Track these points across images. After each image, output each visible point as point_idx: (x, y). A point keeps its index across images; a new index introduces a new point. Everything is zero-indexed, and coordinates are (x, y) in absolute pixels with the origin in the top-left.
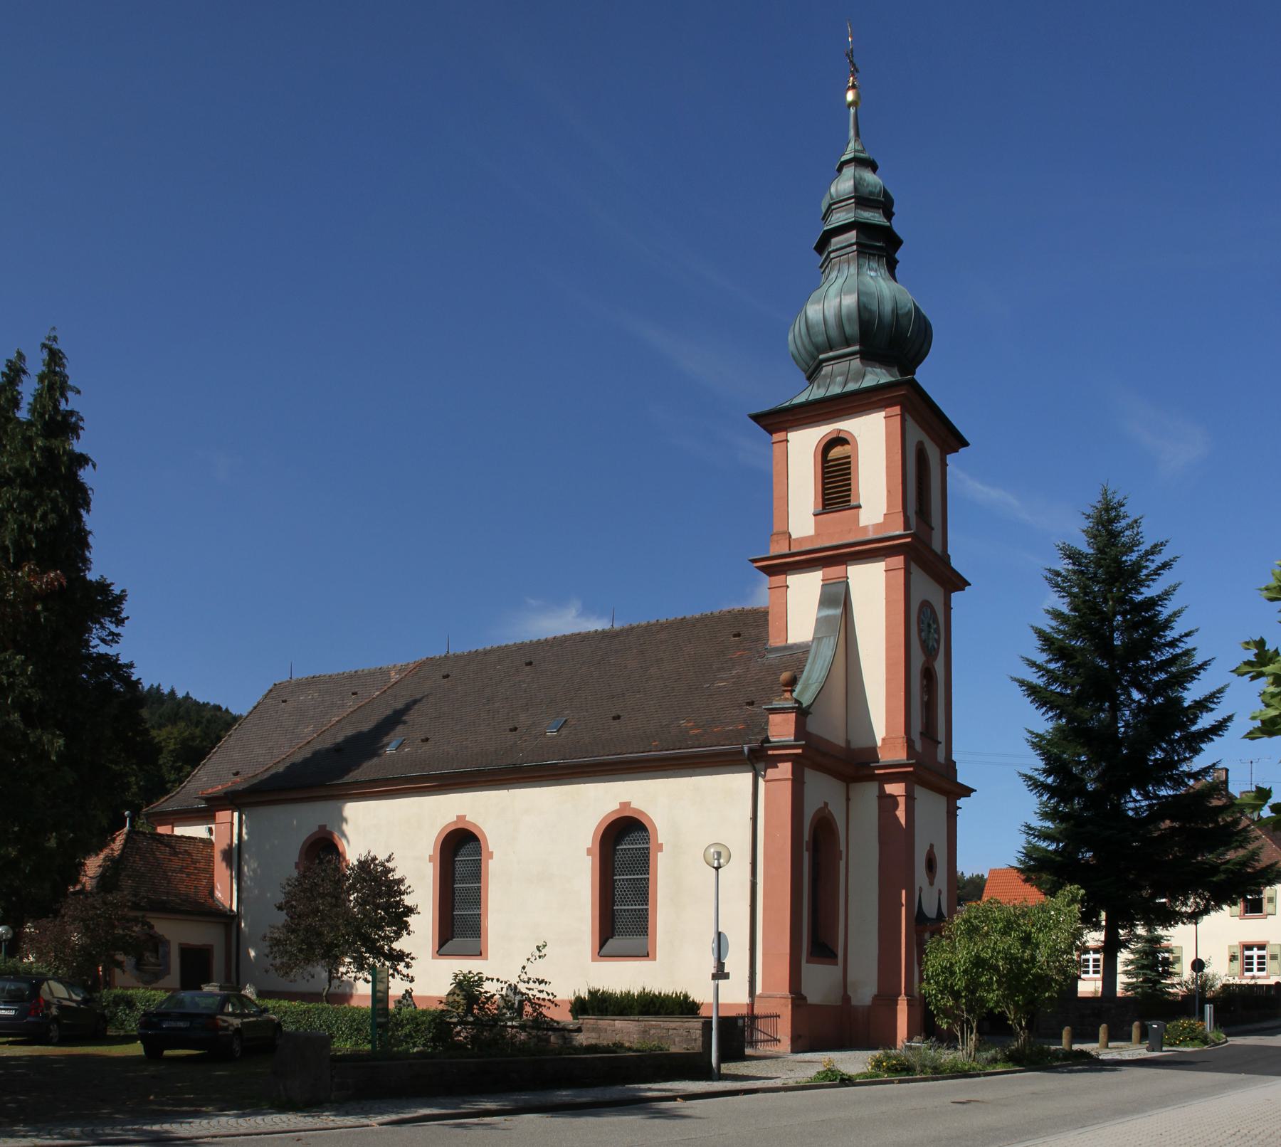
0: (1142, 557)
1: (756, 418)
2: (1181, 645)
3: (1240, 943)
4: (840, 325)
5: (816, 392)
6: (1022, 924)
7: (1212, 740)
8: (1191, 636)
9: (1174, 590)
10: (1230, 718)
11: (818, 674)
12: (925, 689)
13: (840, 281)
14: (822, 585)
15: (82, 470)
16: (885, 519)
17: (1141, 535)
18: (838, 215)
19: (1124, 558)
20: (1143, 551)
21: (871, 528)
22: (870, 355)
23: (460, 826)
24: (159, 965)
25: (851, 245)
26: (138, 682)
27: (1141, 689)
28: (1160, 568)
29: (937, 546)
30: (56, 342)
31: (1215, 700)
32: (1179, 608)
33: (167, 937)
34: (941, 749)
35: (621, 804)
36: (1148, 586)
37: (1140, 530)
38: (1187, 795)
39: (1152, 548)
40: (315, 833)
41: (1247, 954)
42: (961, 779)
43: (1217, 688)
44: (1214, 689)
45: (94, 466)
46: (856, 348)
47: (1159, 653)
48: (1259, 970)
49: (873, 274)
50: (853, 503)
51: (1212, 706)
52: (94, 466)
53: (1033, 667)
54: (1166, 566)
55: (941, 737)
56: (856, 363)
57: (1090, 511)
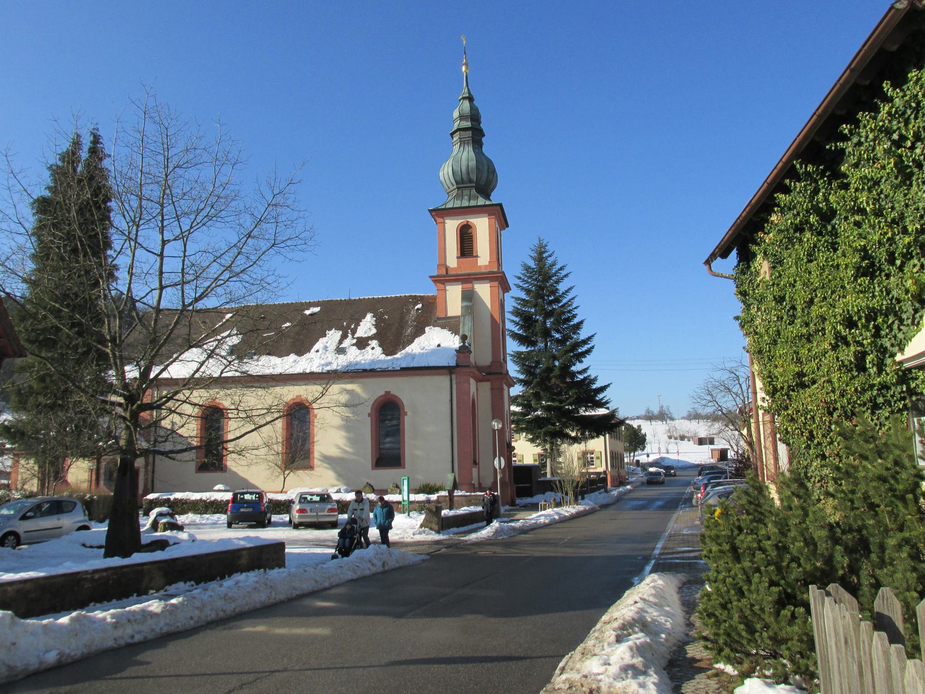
1: (431, 211)
4: (468, 173)
5: (458, 204)
6: (831, 482)
26: (585, 357)
54: (566, 276)
56: (474, 191)
57: (533, 248)
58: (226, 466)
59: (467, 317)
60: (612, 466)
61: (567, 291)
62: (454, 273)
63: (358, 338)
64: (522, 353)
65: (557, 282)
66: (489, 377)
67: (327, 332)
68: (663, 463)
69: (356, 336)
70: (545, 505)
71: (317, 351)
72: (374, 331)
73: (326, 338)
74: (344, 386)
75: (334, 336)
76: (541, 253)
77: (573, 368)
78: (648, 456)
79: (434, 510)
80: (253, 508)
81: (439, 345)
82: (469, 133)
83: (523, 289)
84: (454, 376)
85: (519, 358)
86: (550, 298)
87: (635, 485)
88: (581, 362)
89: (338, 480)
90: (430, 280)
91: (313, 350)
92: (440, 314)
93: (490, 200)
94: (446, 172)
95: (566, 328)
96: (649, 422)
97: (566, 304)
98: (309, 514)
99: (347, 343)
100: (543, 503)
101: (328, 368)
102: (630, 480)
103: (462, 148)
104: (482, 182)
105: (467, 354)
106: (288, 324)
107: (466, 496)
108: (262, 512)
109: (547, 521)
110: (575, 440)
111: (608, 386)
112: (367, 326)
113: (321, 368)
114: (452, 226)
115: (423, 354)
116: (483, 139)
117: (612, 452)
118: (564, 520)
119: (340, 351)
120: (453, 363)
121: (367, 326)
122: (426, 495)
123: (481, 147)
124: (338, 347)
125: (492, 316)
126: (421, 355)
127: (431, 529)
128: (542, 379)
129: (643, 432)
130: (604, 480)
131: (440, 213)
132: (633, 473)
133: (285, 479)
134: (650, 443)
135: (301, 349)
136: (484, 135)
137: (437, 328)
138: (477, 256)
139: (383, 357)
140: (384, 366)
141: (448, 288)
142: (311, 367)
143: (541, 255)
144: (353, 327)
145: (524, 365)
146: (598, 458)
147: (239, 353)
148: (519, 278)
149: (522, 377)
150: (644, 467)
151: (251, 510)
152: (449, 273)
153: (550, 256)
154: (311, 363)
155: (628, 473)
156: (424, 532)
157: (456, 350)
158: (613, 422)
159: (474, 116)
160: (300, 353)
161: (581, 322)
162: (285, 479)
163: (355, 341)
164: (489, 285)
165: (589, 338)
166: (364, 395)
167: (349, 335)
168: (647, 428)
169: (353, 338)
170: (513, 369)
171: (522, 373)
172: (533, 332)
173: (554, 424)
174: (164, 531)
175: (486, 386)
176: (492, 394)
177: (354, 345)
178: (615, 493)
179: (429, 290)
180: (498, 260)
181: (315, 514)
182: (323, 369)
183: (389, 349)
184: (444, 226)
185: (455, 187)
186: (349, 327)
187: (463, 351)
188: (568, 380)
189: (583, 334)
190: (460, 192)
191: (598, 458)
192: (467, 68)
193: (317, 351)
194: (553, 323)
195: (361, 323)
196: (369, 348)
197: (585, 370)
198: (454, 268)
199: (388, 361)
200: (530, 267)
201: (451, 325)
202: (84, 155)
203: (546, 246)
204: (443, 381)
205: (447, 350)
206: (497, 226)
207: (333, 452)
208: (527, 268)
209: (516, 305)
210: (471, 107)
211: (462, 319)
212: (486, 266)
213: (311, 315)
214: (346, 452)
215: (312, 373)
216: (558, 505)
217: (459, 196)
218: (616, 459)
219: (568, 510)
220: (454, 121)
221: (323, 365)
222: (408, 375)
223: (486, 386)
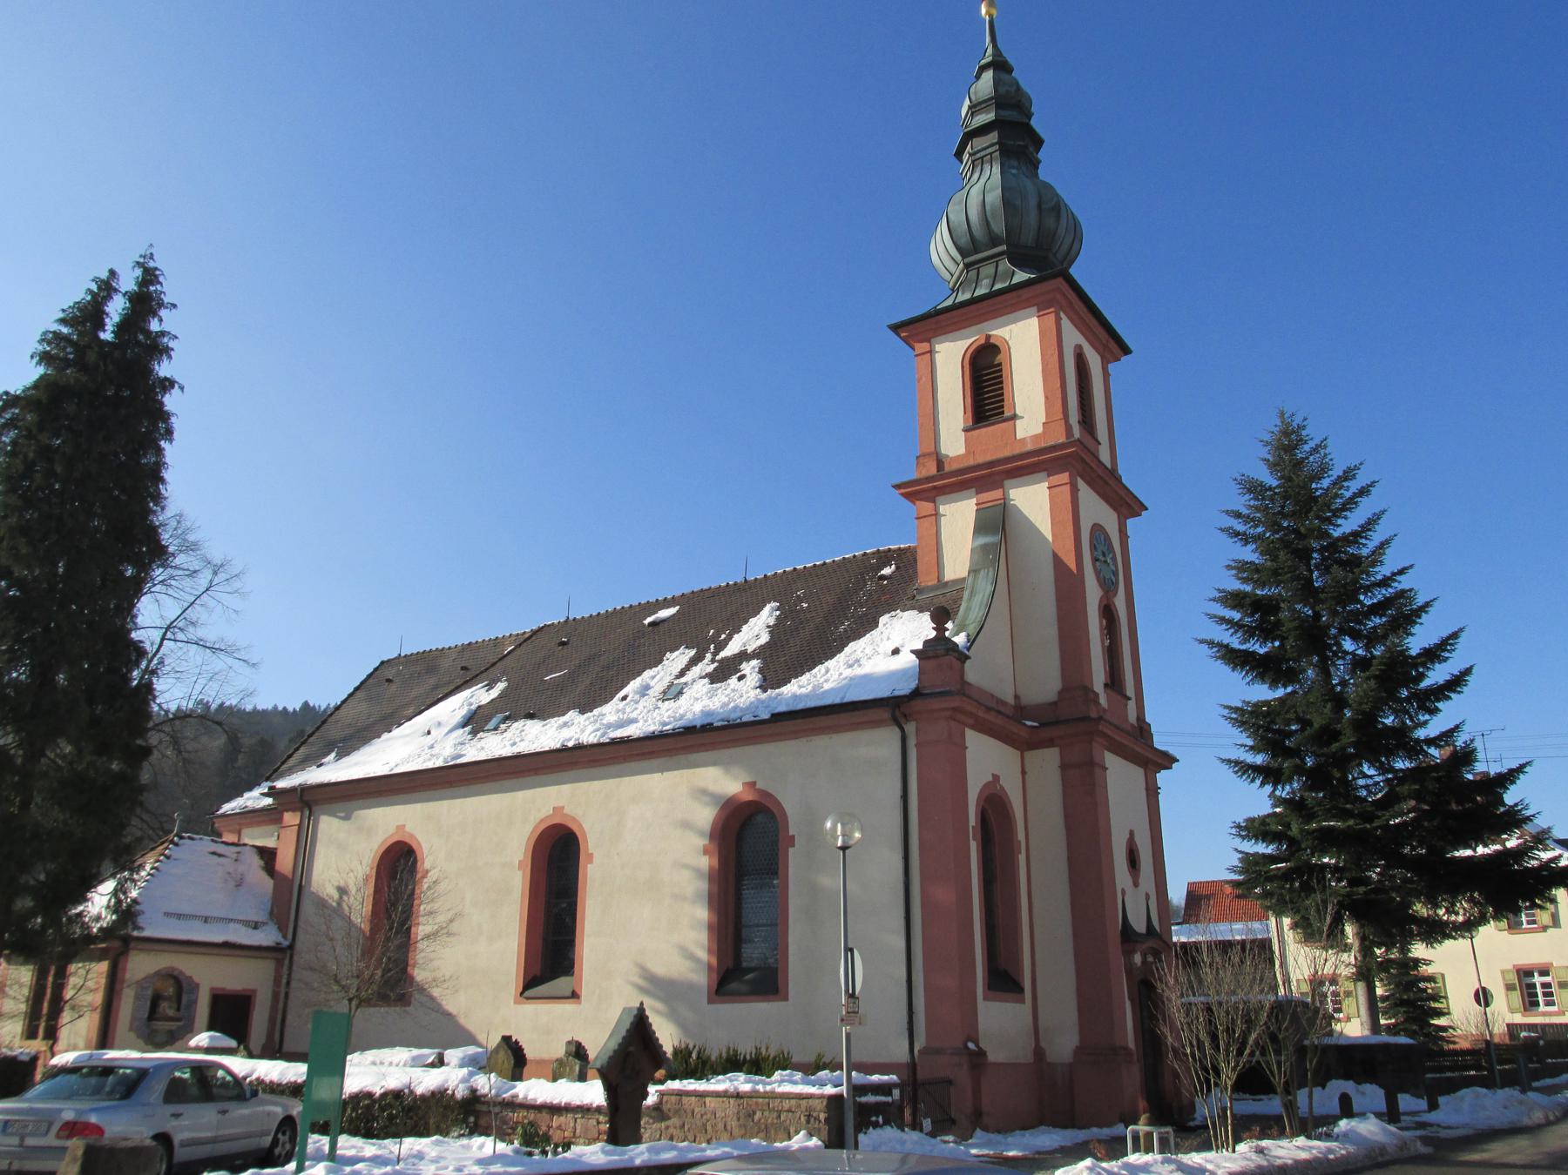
1: (896, 328)
2: (1395, 584)
3: (1514, 966)
4: (986, 223)
7: (1450, 698)
8: (1405, 573)
9: (1383, 514)
10: (1468, 671)
11: (976, 613)
12: (1105, 632)
13: (982, 181)
14: (977, 510)
15: (167, 396)
17: (1329, 457)
18: (978, 118)
19: (1314, 486)
20: (1335, 477)
21: (1029, 440)
22: (1019, 261)
23: (557, 820)
24: (178, 1020)
27: (1355, 636)
28: (1355, 495)
29: (1105, 456)
30: (154, 260)
31: (1449, 648)
32: (1387, 536)
33: (196, 979)
34: (1132, 705)
36: (1346, 518)
37: (1327, 452)
39: (1345, 472)
41: (1528, 985)
42: (1160, 743)
43: (1450, 632)
44: (1445, 634)
45: (182, 388)
46: (1004, 248)
47: (1370, 594)
48: (1548, 1004)
49: (1014, 171)
50: (1007, 414)
51: (1447, 655)
52: (182, 388)
53: (1222, 624)
54: (1364, 492)
55: (1130, 691)
56: (1005, 264)
57: (1267, 437)
83: (1245, 539)
84: (910, 728)
104: (1028, 237)
107: (738, 1095)
111: (1520, 769)
114: (950, 355)
121: (755, 631)
138: (1014, 417)
141: (942, 509)
148: (1238, 515)
152: (947, 469)
175: (1047, 761)
176: (1063, 779)
193: (624, 698)
202: (116, 308)
208: (1254, 488)
212: (1036, 437)
215: (579, 747)
222: (795, 735)
223: (1047, 761)
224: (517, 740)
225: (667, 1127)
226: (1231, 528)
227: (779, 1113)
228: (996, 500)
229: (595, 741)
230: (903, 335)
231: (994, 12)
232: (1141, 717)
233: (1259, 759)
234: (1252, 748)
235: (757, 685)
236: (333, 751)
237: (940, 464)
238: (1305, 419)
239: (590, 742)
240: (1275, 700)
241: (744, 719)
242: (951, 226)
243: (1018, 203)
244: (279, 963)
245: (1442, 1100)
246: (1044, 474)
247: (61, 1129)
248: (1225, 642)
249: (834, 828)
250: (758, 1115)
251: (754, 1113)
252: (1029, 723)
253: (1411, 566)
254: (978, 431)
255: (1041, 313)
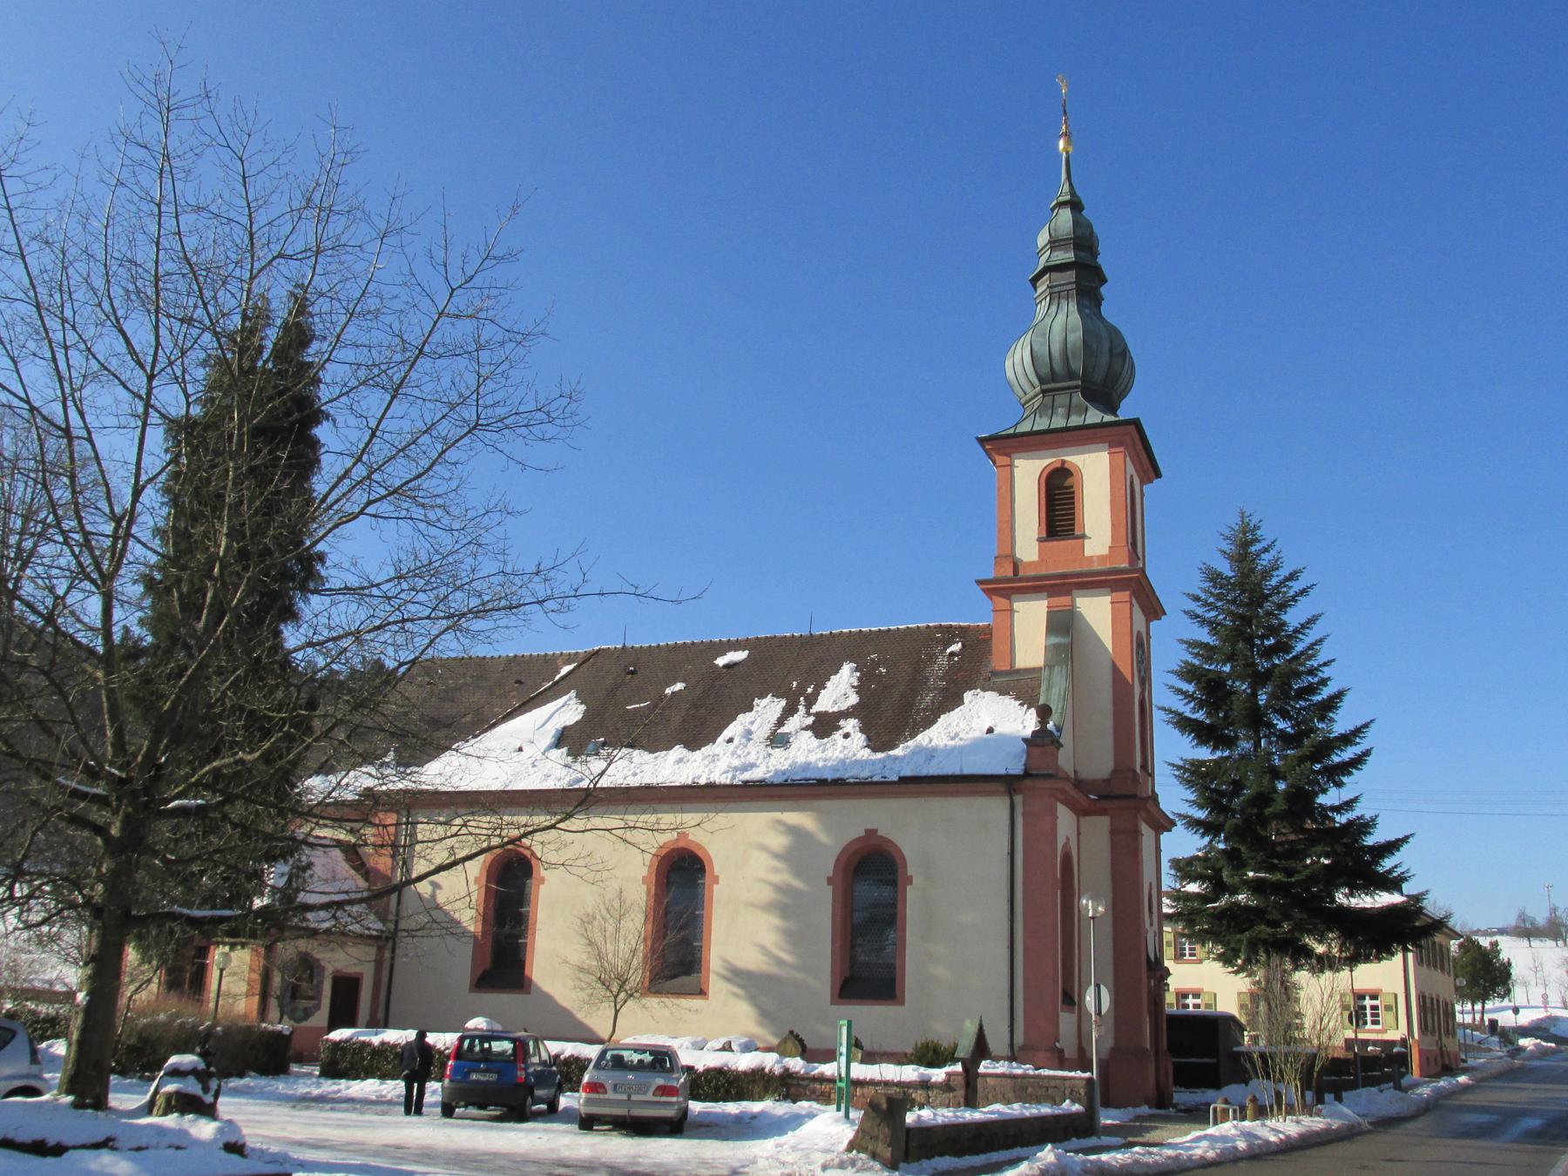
0: (1281, 583)
1: (982, 441)
2: (1320, 674)
4: (1066, 359)
5: (1042, 424)
16: (1110, 551)
18: (1056, 253)
20: (1282, 577)
21: (1095, 559)
23: (681, 844)
25: (1071, 283)
26: (1350, 773)
28: (1297, 595)
32: (1321, 636)
35: (866, 831)
36: (1311, 629)
38: (1324, 829)
39: (1291, 574)
40: (860, 839)
44: (1359, 724)
46: (1079, 383)
50: (1077, 533)
54: (1303, 592)
56: (1078, 397)
57: (1227, 532)
58: (530, 980)
59: (1057, 669)
60: (1424, 1029)
61: (1303, 626)
62: (1031, 573)
63: (817, 715)
64: (1202, 763)
65: (1282, 606)
66: (1105, 804)
67: (756, 701)
68: (1553, 1030)
69: (815, 709)
70: (1225, 1111)
71: (730, 740)
72: (854, 699)
73: (753, 713)
74: (778, 815)
75: (768, 709)
76: (1245, 545)
77: (1322, 800)
78: (1516, 1010)
79: (884, 1106)
80: (498, 1072)
81: (990, 730)
82: (1071, 275)
83: (1203, 621)
84: (1018, 799)
85: (1194, 774)
86: (1266, 643)
87: (1478, 1075)
88: (1339, 785)
89: (760, 1024)
90: (978, 589)
91: (720, 739)
92: (998, 662)
93: (1117, 416)
94: (1018, 361)
95: (1304, 708)
96: (1525, 942)
97: (1302, 653)
98: (611, 1095)
99: (793, 724)
100: (1220, 1106)
101: (747, 776)
102: (1471, 1062)
103: (1054, 308)
104: (1098, 376)
105: (1053, 748)
106: (679, 686)
107: (1014, 1077)
108: (518, 1085)
109: (1211, 1154)
110: (1324, 964)
111: (1405, 840)
112: (840, 690)
113: (730, 775)
114: (1028, 472)
115: (953, 749)
116: (1103, 290)
117: (1422, 998)
118: (1261, 1154)
119: (778, 740)
120: (1017, 768)
121: (840, 690)
122: (922, 1070)
123: (1099, 304)
124: (774, 733)
125: (1114, 666)
126: (949, 752)
127: (874, 1156)
128: (1247, 821)
129: (1504, 956)
130: (1402, 1060)
131: (1003, 445)
132: (1480, 1047)
133: (617, 1012)
134: (1525, 984)
135: (698, 734)
136: (1104, 281)
137: (989, 694)
138: (1083, 537)
139: (866, 754)
140: (864, 774)
141: (1016, 605)
142: (711, 772)
143: (1244, 547)
144: (810, 690)
145: (1207, 788)
146: (1388, 1008)
147: (571, 741)
148: (1197, 599)
149: (1201, 814)
150: (1507, 1036)
151: (493, 1077)
153: (1266, 550)
154: (712, 766)
155: (1466, 1048)
156: (853, 1163)
157: (1025, 740)
158: (1417, 924)
159: (1083, 241)
160: (693, 744)
161: (1340, 695)
162: (617, 1012)
163: (810, 720)
164: (1108, 599)
165: (1358, 731)
166: (824, 838)
167: (800, 707)
168: (1512, 951)
169: (808, 714)
170: (1174, 797)
171: (1201, 807)
172: (1226, 716)
173: (1275, 924)
174: (165, 1114)
177: (806, 728)
178: (1425, 1091)
179: (976, 612)
180: (1134, 544)
181: (625, 1097)
182: (734, 777)
183: (880, 738)
184: (1012, 473)
185: (1038, 389)
186: (801, 690)
187: (1041, 741)
188: (1309, 825)
189: (1342, 722)
190: (1048, 399)
191: (1388, 1008)
192: (1068, 143)
193: (730, 740)
194: (1272, 696)
195: (828, 684)
196: (838, 735)
197: (1348, 805)
198: (1031, 563)
199: (874, 763)
200: (1219, 575)
201: (1022, 687)
203: (1257, 528)
204: (995, 809)
205: (1006, 739)
206: (1131, 469)
207: (751, 960)
208: (1214, 577)
209: (1189, 658)
210: (1076, 223)
211: (1045, 674)
212: (1101, 557)
213: (727, 666)
214: (780, 962)
215: (711, 786)
216: (1261, 1112)
217: (1048, 409)
218: (1434, 1014)
219: (1284, 1127)
220: (1039, 254)
221: (736, 769)
222: (917, 794)
224: (638, 771)
225: (955, 1097)
226: (1193, 611)
227: (1047, 1088)
228: (1132, 650)
229: (728, 782)
230: (988, 447)
231: (1070, 150)
232: (1153, 790)
233: (1201, 814)
234: (1194, 802)
235: (865, 744)
236: (390, 751)
237: (1016, 565)
238: (1261, 521)
239: (723, 782)
240: (1209, 761)
241: (875, 779)
242: (1034, 355)
243: (1094, 346)
244: (380, 949)
245: (1345, 1094)
246: (1108, 590)
247: (656, 1089)
248: (1180, 711)
249: (1087, 905)
250: (1030, 1090)
251: (1027, 1088)
252: (1092, 797)
253: (1334, 660)
254: (1050, 544)
255: (1113, 450)
